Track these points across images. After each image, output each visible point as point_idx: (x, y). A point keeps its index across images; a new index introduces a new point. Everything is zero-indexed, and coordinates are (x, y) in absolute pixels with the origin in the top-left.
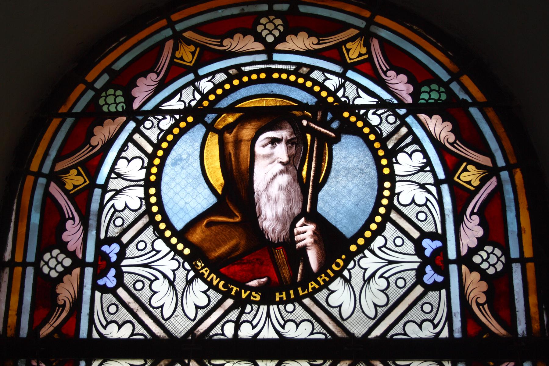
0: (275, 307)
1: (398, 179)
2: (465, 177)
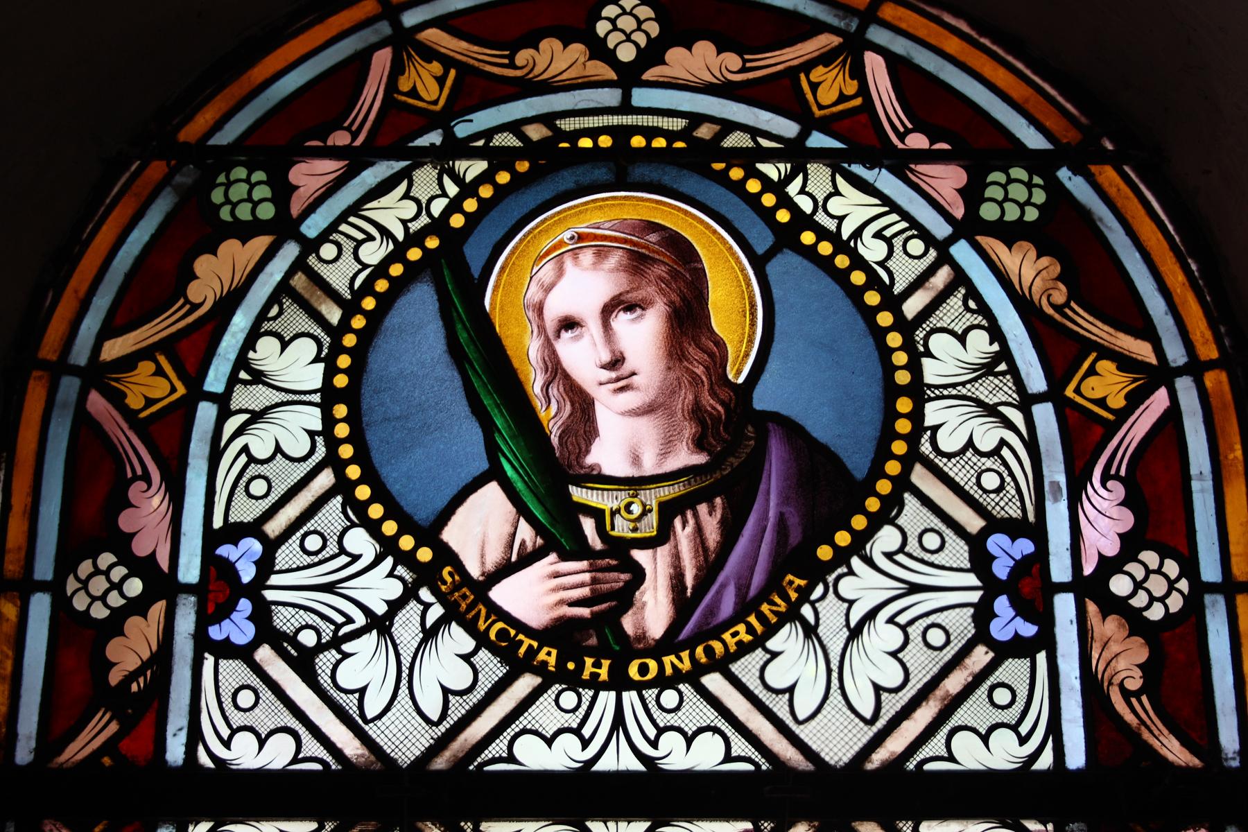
0: (634, 694)
2: (1094, 388)
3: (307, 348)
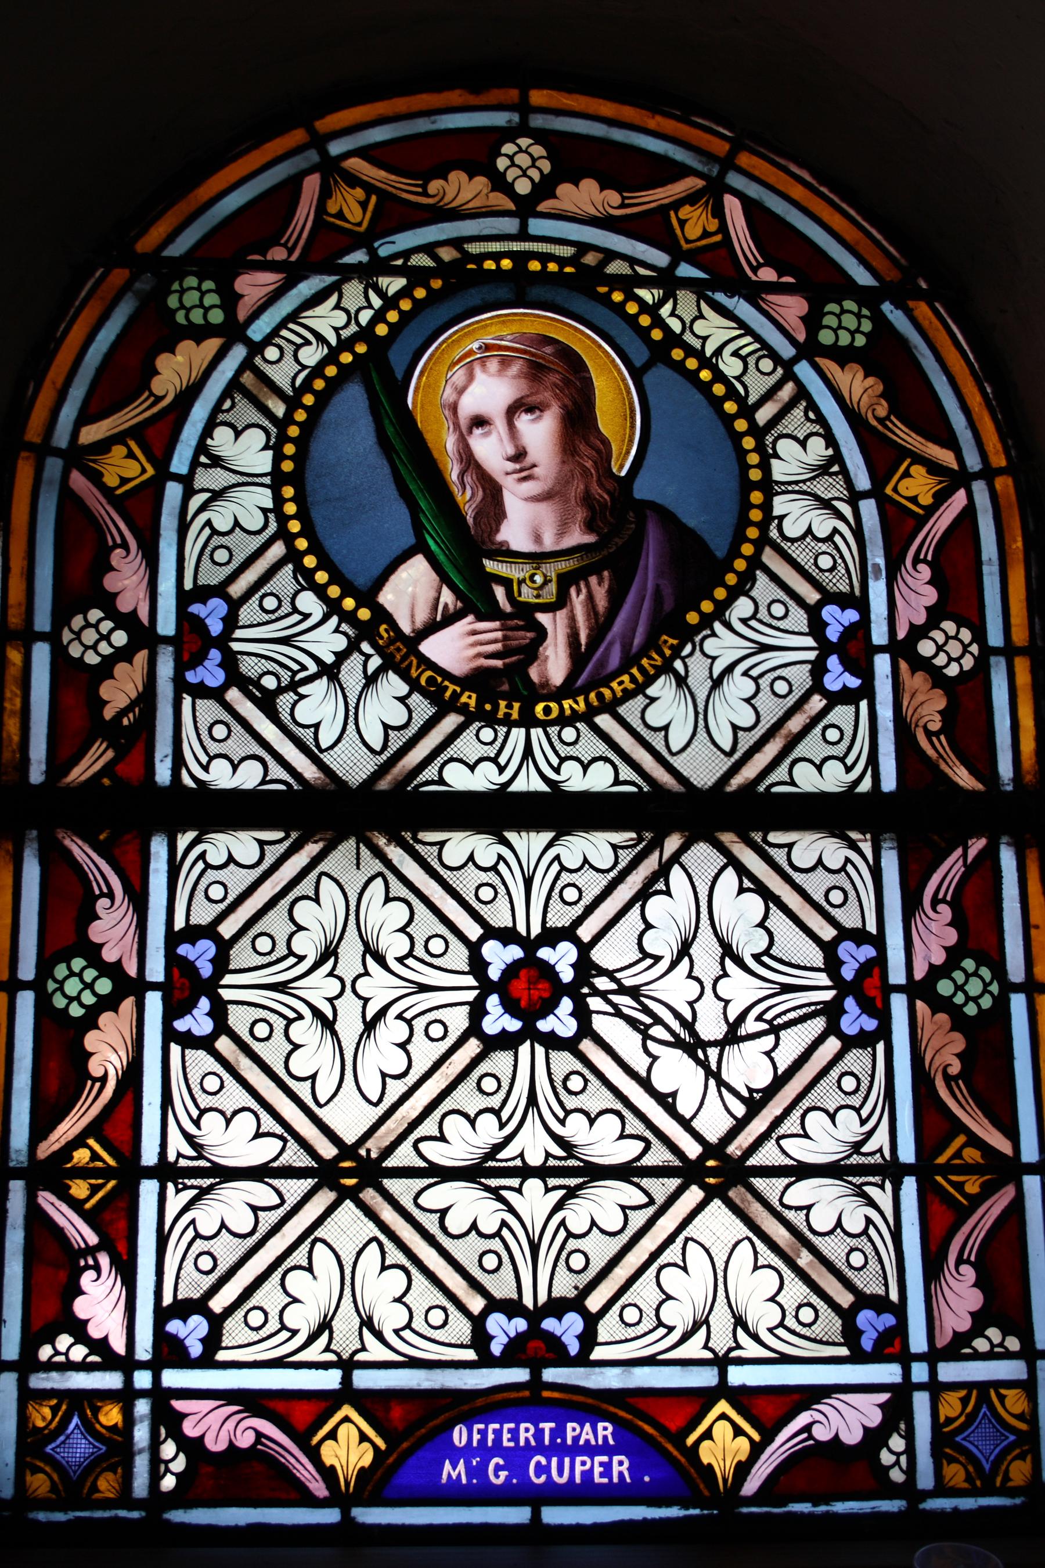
0: (540, 730)
1: (267, 480)
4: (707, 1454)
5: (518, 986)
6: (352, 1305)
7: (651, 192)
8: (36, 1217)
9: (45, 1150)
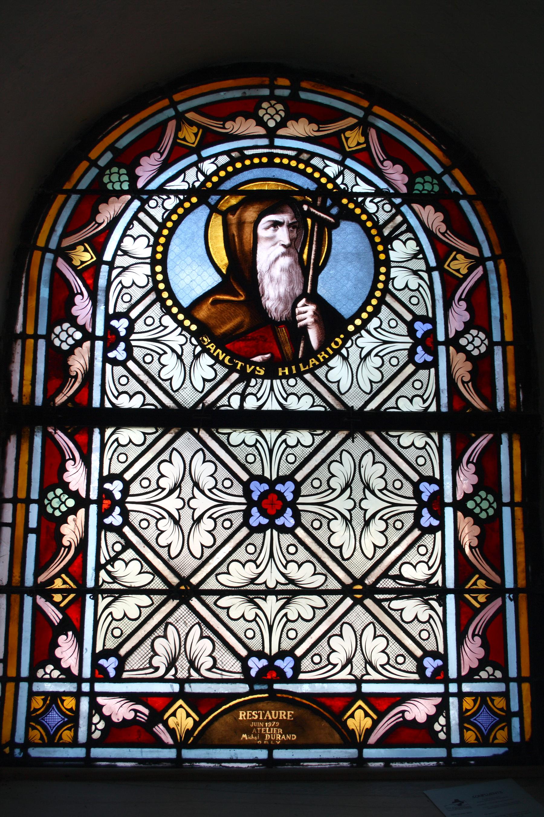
2: (455, 265)
3: (143, 241)
4: (351, 724)
5: (265, 504)
6: (198, 651)
7: (455, 238)
8: (36, 609)
9: (42, 578)
